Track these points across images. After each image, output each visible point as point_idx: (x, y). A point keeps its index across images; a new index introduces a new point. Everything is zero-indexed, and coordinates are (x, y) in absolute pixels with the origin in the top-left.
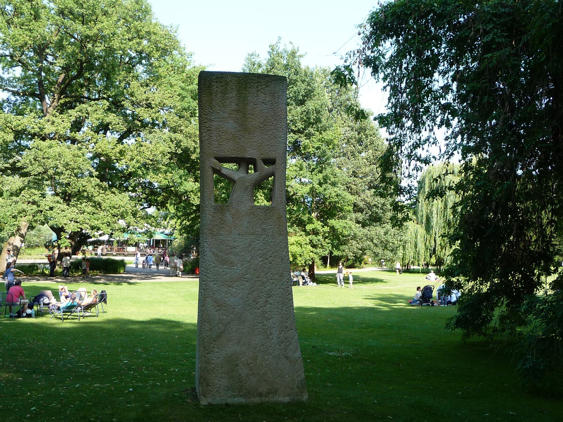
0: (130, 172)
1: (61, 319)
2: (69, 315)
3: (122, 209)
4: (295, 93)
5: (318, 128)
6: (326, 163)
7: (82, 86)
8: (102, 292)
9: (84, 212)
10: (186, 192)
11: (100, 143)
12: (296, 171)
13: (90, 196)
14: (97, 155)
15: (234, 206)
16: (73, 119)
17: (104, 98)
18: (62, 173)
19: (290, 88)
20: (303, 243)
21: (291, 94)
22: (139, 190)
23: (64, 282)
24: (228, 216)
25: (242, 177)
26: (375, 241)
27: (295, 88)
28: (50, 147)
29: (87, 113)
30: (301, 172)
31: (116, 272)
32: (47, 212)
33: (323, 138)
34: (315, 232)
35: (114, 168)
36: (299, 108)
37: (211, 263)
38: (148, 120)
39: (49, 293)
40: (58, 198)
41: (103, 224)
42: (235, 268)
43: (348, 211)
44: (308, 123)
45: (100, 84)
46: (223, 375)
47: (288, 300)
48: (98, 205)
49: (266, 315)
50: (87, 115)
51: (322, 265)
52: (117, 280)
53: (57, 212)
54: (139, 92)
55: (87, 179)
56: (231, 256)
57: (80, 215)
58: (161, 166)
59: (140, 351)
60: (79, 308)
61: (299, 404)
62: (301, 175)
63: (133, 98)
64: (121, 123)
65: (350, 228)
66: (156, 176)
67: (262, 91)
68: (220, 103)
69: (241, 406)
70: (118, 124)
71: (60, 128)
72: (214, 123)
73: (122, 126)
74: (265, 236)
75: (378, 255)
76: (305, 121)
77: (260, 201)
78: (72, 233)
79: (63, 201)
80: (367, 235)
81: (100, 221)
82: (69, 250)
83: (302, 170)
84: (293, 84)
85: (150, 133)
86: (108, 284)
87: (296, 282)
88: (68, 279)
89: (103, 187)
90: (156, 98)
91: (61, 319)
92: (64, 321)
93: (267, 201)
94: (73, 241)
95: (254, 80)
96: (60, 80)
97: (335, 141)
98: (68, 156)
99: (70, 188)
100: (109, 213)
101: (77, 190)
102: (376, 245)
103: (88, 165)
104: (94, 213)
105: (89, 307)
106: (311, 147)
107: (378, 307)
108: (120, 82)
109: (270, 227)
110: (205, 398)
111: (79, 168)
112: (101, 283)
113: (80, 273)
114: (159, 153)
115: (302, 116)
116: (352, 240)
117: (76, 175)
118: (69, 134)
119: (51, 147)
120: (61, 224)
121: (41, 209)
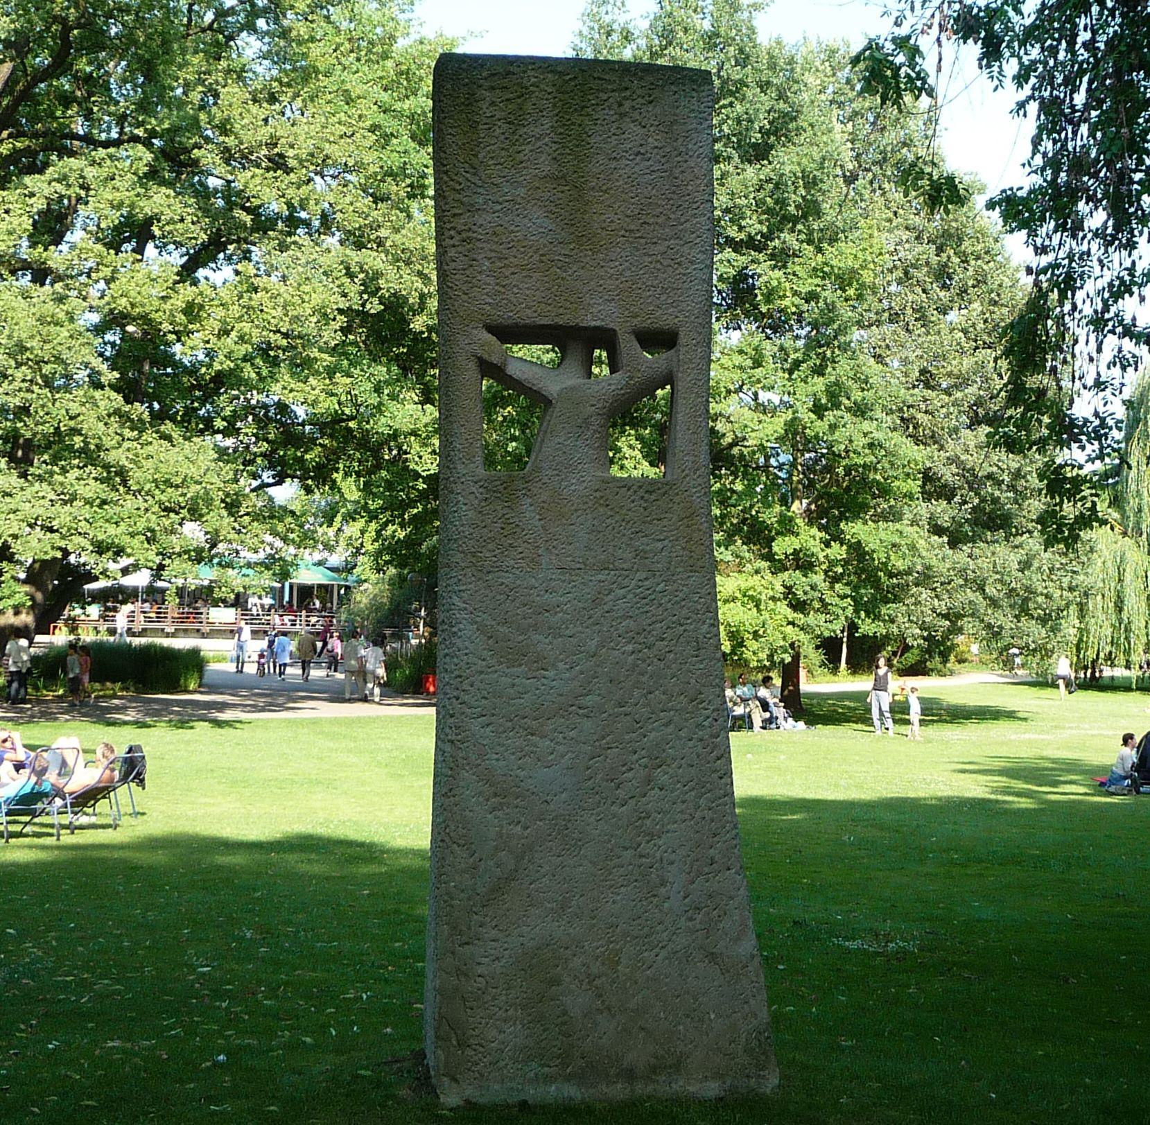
2: (26, 824)
3: (193, 490)
4: (739, 122)
5: (810, 232)
6: (836, 343)
7: (66, 100)
10: (395, 436)
11: (124, 280)
12: (741, 368)
14: (115, 320)
15: (545, 480)
16: (39, 204)
17: (135, 139)
20: (763, 597)
24: (528, 513)
25: (572, 388)
27: (739, 108)
29: (82, 187)
30: (759, 372)
31: (174, 687)
33: (826, 264)
34: (802, 562)
35: (169, 360)
36: (750, 172)
37: (472, 659)
41: (132, 535)
42: (551, 674)
43: (905, 496)
44: (780, 219)
45: (125, 95)
48: (117, 477)
49: (648, 822)
50: (83, 193)
51: (823, 665)
52: (178, 713)
54: (246, 121)
55: (81, 393)
57: (60, 509)
58: (315, 353)
59: (248, 935)
60: (58, 802)
63: (227, 140)
64: (189, 219)
65: (913, 547)
66: (301, 384)
67: (636, 115)
68: (503, 153)
70: (182, 220)
73: (193, 227)
75: (999, 633)
76: (769, 211)
78: (37, 565)
79: (8, 463)
80: (965, 570)
83: (760, 365)
84: (732, 94)
85: (283, 248)
86: (150, 726)
87: (741, 717)
88: (22, 711)
89: (132, 421)
90: (302, 138)
93: (652, 464)
97: (864, 273)
98: (22, 324)
99: (30, 422)
101: (52, 430)
102: (994, 603)
104: (104, 502)
107: (1000, 797)
108: (187, 86)
109: (660, 545)
111: (58, 359)
112: (125, 723)
113: (61, 692)
115: (761, 195)
116: (917, 585)
117: (48, 383)
118: (25, 252)
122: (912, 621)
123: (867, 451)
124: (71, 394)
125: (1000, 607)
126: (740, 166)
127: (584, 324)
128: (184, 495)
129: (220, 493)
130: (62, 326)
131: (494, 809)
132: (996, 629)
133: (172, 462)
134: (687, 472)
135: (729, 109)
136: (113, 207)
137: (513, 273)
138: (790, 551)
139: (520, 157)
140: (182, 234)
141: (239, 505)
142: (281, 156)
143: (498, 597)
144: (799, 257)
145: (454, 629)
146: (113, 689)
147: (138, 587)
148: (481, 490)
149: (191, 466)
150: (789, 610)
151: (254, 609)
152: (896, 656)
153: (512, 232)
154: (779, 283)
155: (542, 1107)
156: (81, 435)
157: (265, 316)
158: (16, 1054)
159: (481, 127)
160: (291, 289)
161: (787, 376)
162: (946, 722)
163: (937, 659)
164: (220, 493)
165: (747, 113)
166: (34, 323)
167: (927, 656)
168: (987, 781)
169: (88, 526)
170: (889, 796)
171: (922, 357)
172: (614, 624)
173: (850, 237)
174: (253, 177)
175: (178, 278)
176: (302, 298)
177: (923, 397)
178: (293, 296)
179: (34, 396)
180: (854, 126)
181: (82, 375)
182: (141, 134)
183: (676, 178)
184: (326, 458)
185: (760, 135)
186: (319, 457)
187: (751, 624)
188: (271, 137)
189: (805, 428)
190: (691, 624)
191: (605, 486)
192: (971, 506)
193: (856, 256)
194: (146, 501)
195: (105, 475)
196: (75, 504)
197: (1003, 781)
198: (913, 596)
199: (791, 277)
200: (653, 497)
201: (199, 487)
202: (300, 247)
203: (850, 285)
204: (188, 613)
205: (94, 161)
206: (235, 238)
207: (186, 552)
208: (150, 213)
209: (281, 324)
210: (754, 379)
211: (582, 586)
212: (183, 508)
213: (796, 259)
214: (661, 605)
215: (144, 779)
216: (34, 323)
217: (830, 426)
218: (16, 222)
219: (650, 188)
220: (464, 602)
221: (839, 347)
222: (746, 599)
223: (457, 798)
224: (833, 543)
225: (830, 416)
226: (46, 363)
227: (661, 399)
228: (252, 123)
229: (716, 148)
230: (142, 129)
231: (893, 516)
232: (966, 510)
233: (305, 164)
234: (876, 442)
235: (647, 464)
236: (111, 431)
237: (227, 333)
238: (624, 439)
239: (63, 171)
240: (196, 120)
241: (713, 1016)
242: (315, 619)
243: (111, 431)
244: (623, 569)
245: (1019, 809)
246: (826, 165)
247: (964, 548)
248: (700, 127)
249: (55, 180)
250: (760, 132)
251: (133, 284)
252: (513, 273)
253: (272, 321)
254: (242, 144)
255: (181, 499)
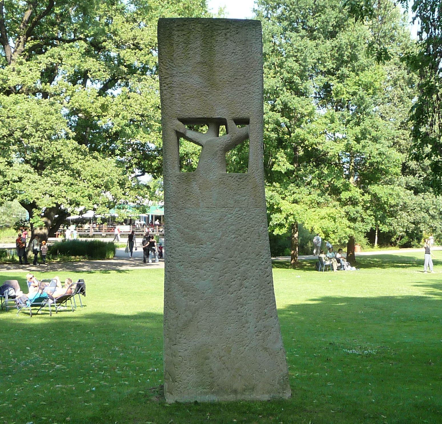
0: (116, 132)
1: (28, 314)
2: (39, 310)
3: (106, 179)
4: (323, 22)
5: (354, 67)
6: (364, 112)
7: (53, 24)
8: (79, 281)
9: (60, 183)
10: (187, 154)
11: (77, 96)
12: (325, 123)
13: (67, 163)
14: (74, 112)
15: (201, 175)
16: (43, 67)
17: (80, 39)
18: (32, 136)
19: (317, 17)
20: (337, 217)
21: (317, 25)
22: (129, 152)
23: (39, 271)
24: (195, 186)
25: (211, 141)
26: (431, 212)
27: (323, 17)
28: (16, 103)
29: (59, 59)
30: (333, 125)
31: (103, 258)
32: (15, 184)
33: (360, 80)
34: (353, 202)
35: (96, 127)
36: (328, 42)
37: (175, 241)
38: (137, 64)
39: (15, 282)
40: (27, 167)
41: (83, 197)
42: (204, 246)
43: (394, 174)
44: (341, 62)
45: (76, 20)
46: (192, 369)
47: (266, 283)
48: (76, 174)
49: (241, 300)
50: (60, 62)
51: (367, 244)
52: (104, 267)
53: (27, 183)
54: (123, 30)
55: (61, 141)
56: (198, 233)
57: (55, 187)
58: (152, 123)
59: (117, 349)
60: (51, 301)
61: (280, 402)
62: (333, 129)
63: (116, 38)
64: (102, 70)
65: (398, 195)
66: (147, 135)
67: (232, 38)
68: (183, 54)
69: (213, 404)
70: (99, 71)
71: (27, 79)
72: (175, 79)
73: (104, 73)
74: (238, 209)
75: (435, 230)
76: (337, 59)
77: (281, 164)
78: (48, 210)
79: (34, 170)
80: (421, 204)
81: (79, 194)
82: (45, 231)
83: (333, 122)
84: (320, 11)
85: (140, 80)
86: (93, 273)
87: (329, 266)
88: (43, 267)
89: (82, 152)
90: (146, 36)
91: (28, 314)
92: (33, 316)
93: (291, 164)
94: (49, 218)
95: (222, 26)
96: (26, 18)
97: (376, 83)
98: (37, 114)
99: (42, 153)
100: (90, 183)
101: (51, 156)
102: (433, 217)
103: (62, 124)
104: (72, 184)
105: (62, 300)
106: (345, 93)
107: (428, 296)
108: (101, 17)
109: (244, 198)
110: (171, 395)
111: (52, 129)
112: (83, 271)
113: (59, 260)
114: (150, 106)
115: (333, 52)
116: (401, 210)
117: (49, 138)
118: (40, 86)
119: (17, 103)
120: (32, 199)
121: (7, 179)
122: (399, 225)
123: (378, 156)
124: (57, 142)
125: (436, 219)
126: (324, 41)
127: (214, 117)
128: (103, 181)
129: (117, 180)
130: (53, 115)
131: (185, 296)
132: (434, 228)
133: (98, 168)
134: (254, 171)
135: (319, 17)
136: (71, 66)
137: (187, 99)
138: (348, 197)
139: (189, 56)
140: (99, 76)
141: (125, 184)
142: (138, 43)
143: (184, 218)
144: (349, 77)
145: (169, 231)
146: (79, 259)
147: (91, 218)
148: (177, 179)
149: (105, 169)
150: (347, 221)
151: (137, 225)
152: (398, 240)
153: (187, 84)
154: (341, 89)
155: (203, 404)
156: (62, 158)
157: (132, 108)
158: (22, 389)
159: (174, 45)
160: (143, 97)
161: (344, 126)
162: (415, 266)
163: (416, 241)
164: (117, 180)
165: (326, 19)
166: (42, 114)
167: (411, 240)
168: (424, 289)
169: (66, 194)
170: (382, 296)
171: (402, 117)
172: (227, 227)
173: (370, 69)
174: (127, 52)
175: (98, 94)
176: (147, 101)
177: (402, 133)
178: (143, 100)
179: (43, 143)
180: (372, 22)
181: (63, 134)
182: (82, 37)
183: (248, 61)
184: (160, 164)
185: (332, 28)
186: (158, 164)
187: (332, 228)
188: (134, 36)
189: (352, 147)
190: (256, 227)
191: (223, 177)
192: (423, 178)
193: (372, 77)
194: (88, 183)
195: (72, 173)
196: (60, 185)
197: (431, 289)
198: (399, 215)
199: (346, 86)
200: (241, 180)
201: (108, 177)
202: (146, 80)
203: (370, 88)
204: (111, 228)
205: (64, 49)
206: (121, 77)
207: (104, 203)
208: (86, 69)
209: (139, 111)
210: (331, 128)
211: (215, 214)
212: (102, 186)
213: (348, 78)
214: (245, 220)
215: (85, 292)
216: (42, 114)
217: (363, 146)
218: (34, 74)
219: (238, 65)
220: (172, 221)
221: (366, 114)
222: (330, 217)
223: (171, 292)
224: (365, 194)
225: (363, 142)
226: (47, 130)
227: (293, 137)
228: (126, 31)
229: (314, 33)
230: (82, 35)
231: (390, 182)
232: (421, 179)
233: (148, 46)
234: (382, 153)
235: (289, 164)
236: (73, 156)
237: (118, 116)
238: (279, 154)
239: (52, 53)
240: (103, 30)
241: (266, 371)
242: (162, 229)
243: (73, 156)
244: (230, 207)
245: (434, 300)
246: (359, 39)
247: (421, 195)
248: (256, 42)
249: (49, 57)
250: (332, 26)
251: (80, 97)
252: (187, 99)
253: (135, 110)
254: (122, 39)
255: (102, 182)
